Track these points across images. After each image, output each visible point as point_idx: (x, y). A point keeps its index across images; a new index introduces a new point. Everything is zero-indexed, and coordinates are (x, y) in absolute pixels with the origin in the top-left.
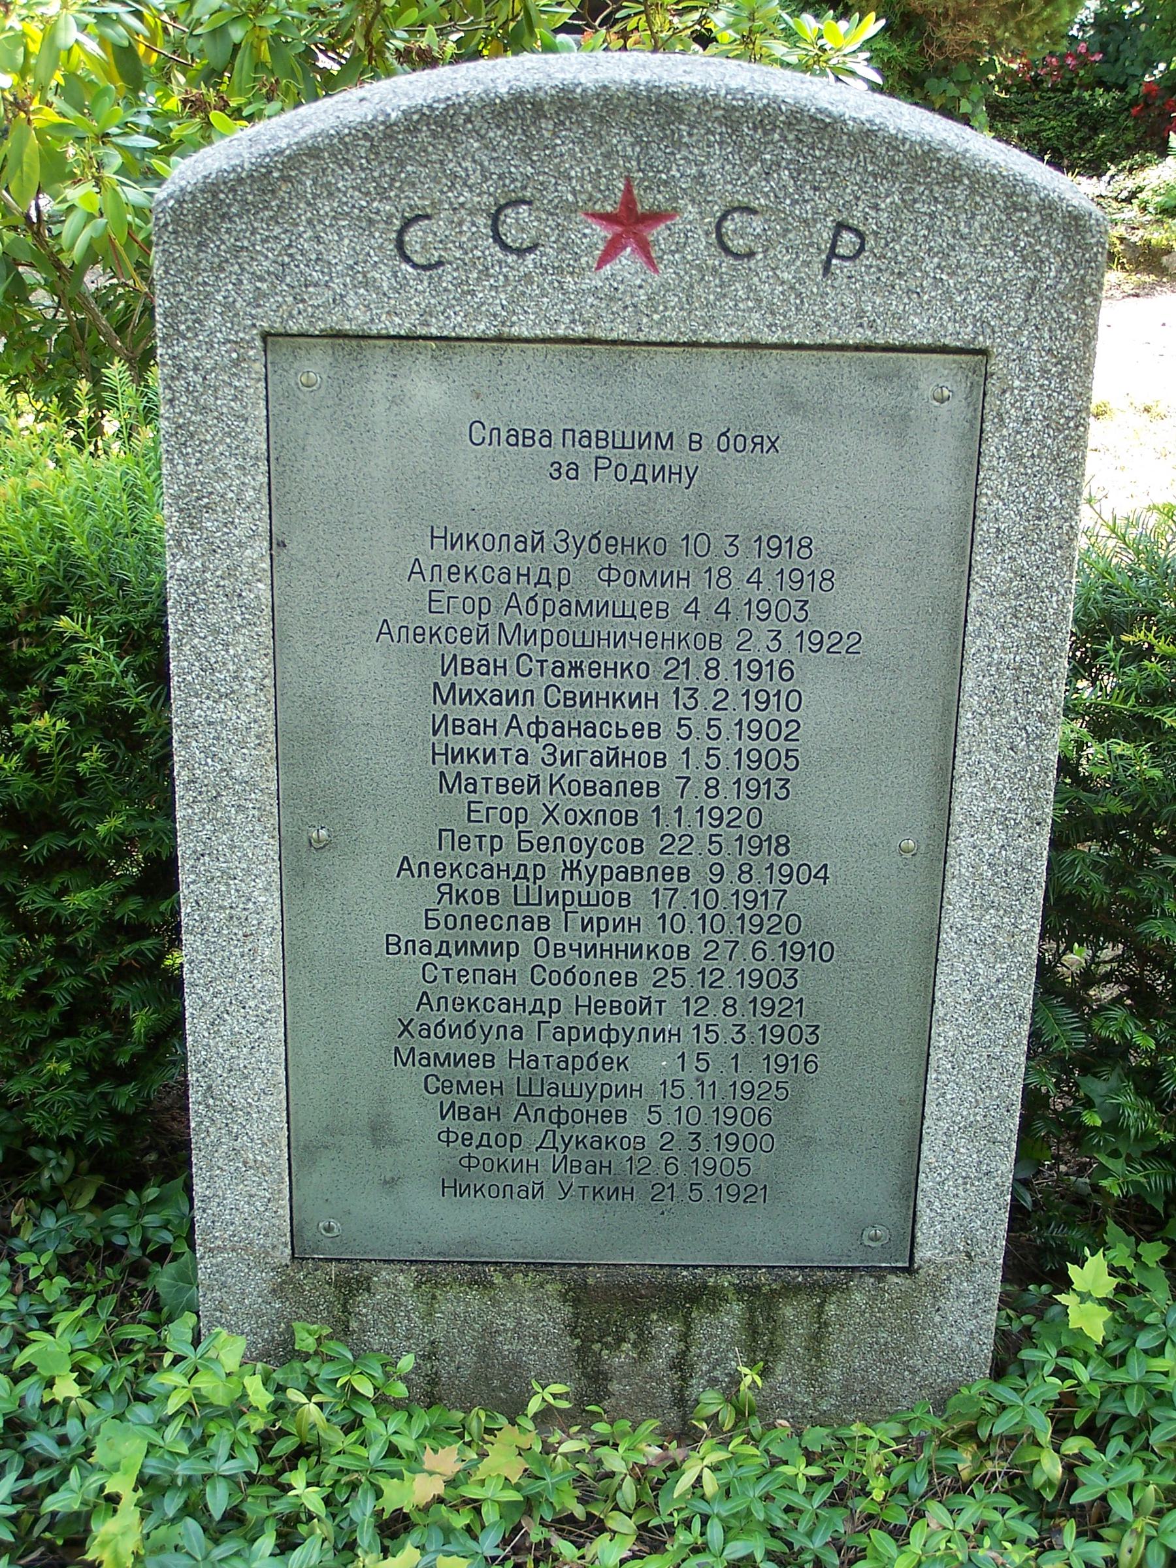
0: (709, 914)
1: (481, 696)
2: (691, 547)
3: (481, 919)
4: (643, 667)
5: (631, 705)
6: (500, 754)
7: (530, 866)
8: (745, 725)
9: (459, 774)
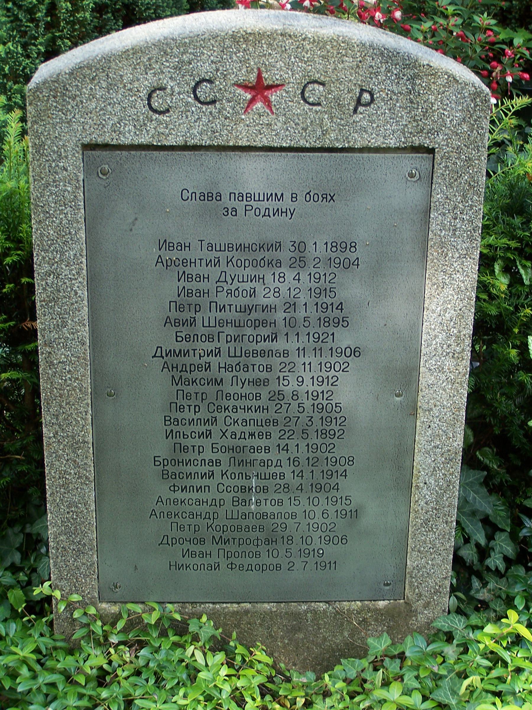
0: (311, 522)
2: (270, 554)
3: (265, 322)
6: (191, 352)
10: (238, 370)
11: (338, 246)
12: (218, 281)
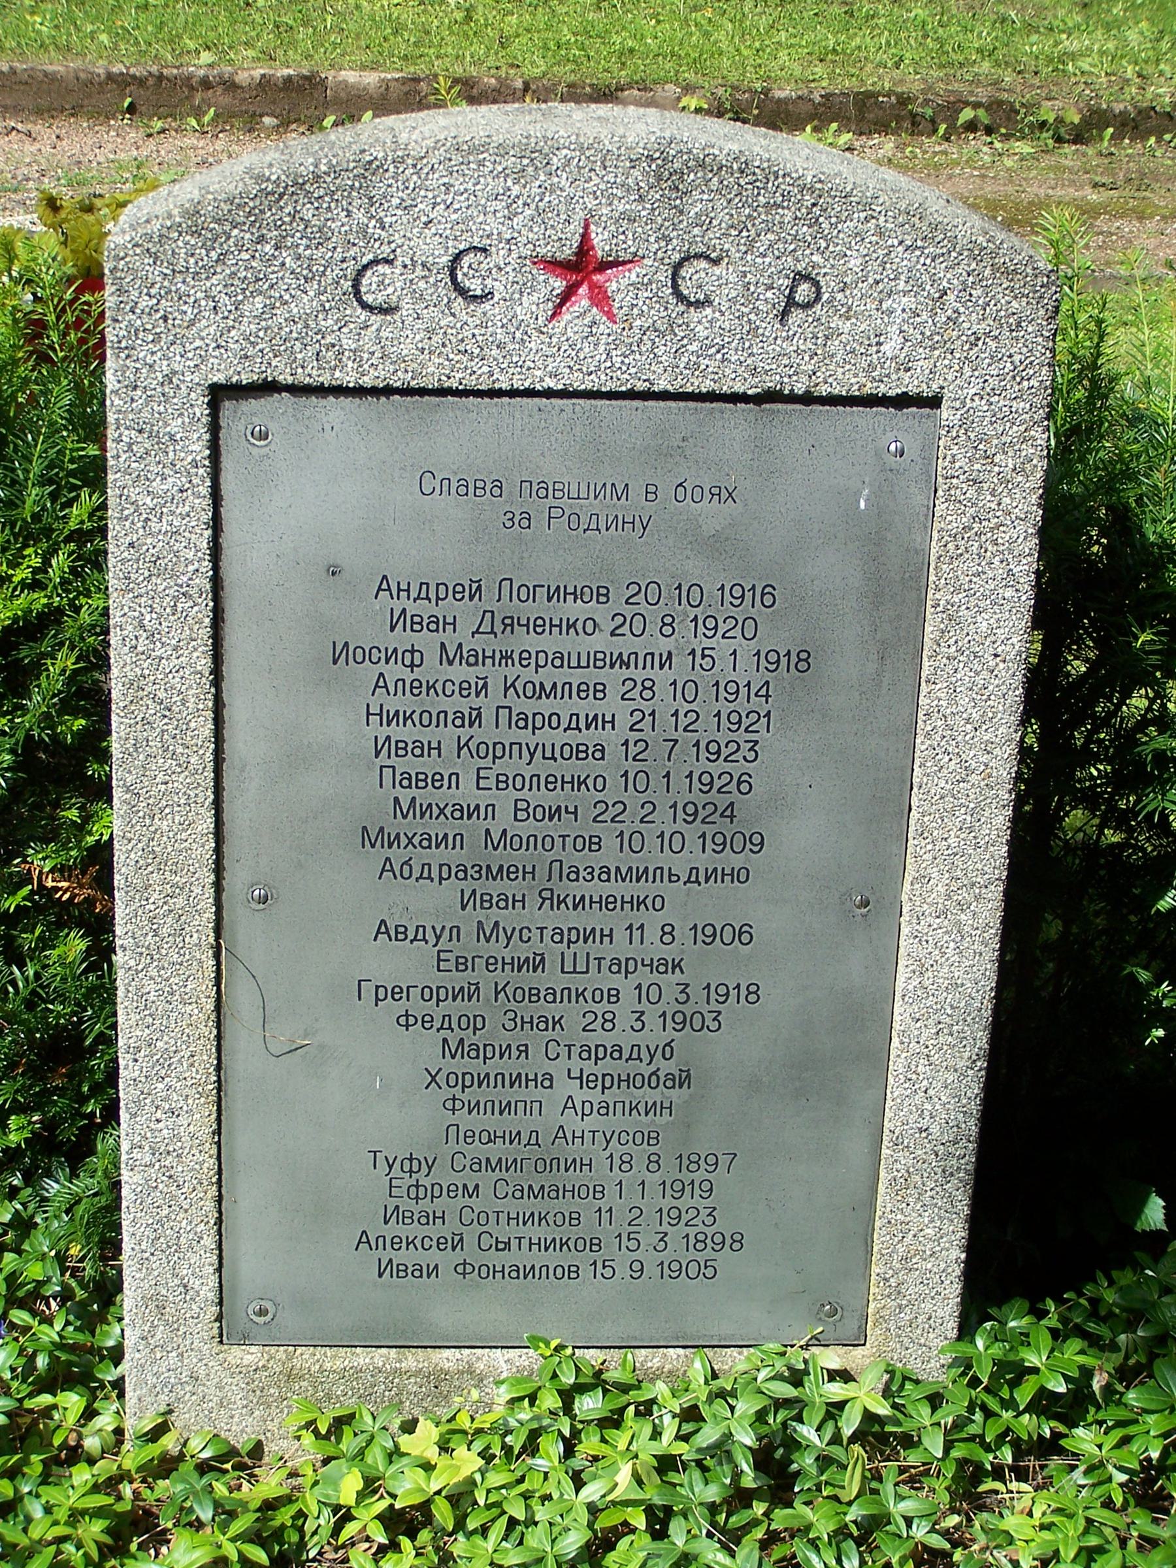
1: (442, 811)
4: (600, 780)
8: (713, 988)
9: (460, 645)
11: (708, 1241)
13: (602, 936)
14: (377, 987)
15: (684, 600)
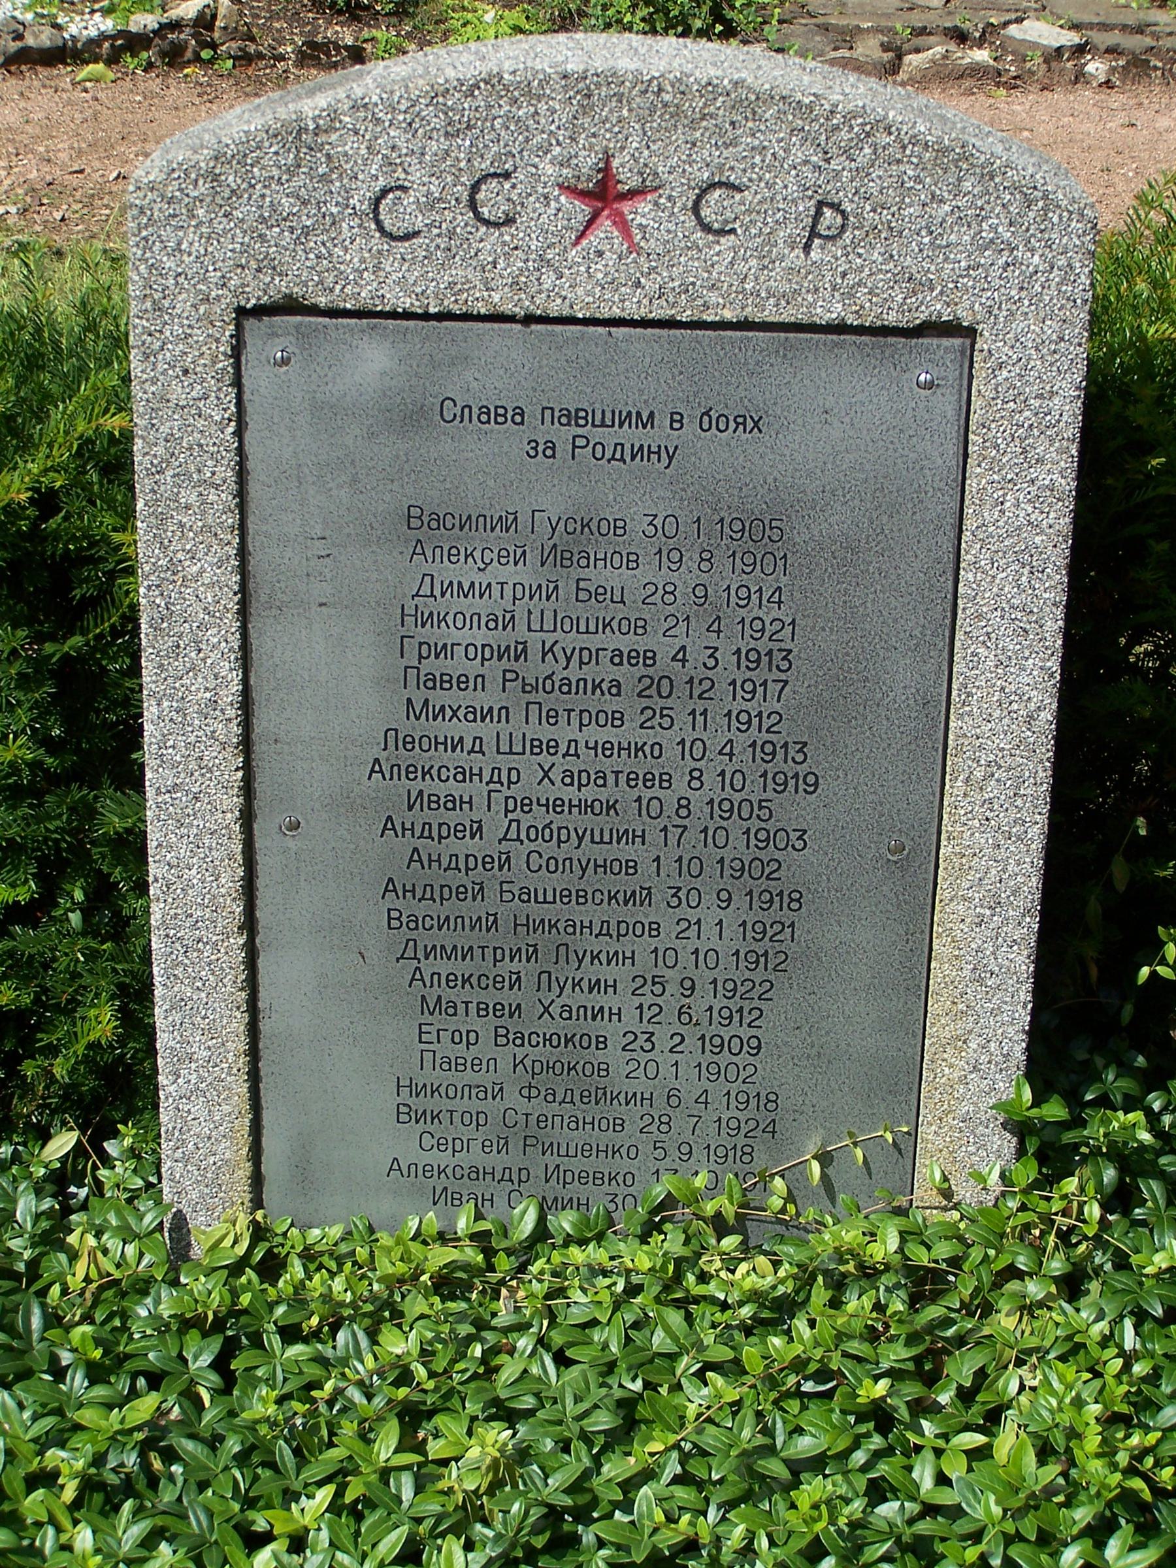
2: (710, 840)
4: (629, 1176)
5: (626, 903)
6: (477, 952)
7: (515, 1170)
10: (548, 688)
12: (402, 957)
13: (611, 1014)
14: (421, 644)
15: (644, 812)
